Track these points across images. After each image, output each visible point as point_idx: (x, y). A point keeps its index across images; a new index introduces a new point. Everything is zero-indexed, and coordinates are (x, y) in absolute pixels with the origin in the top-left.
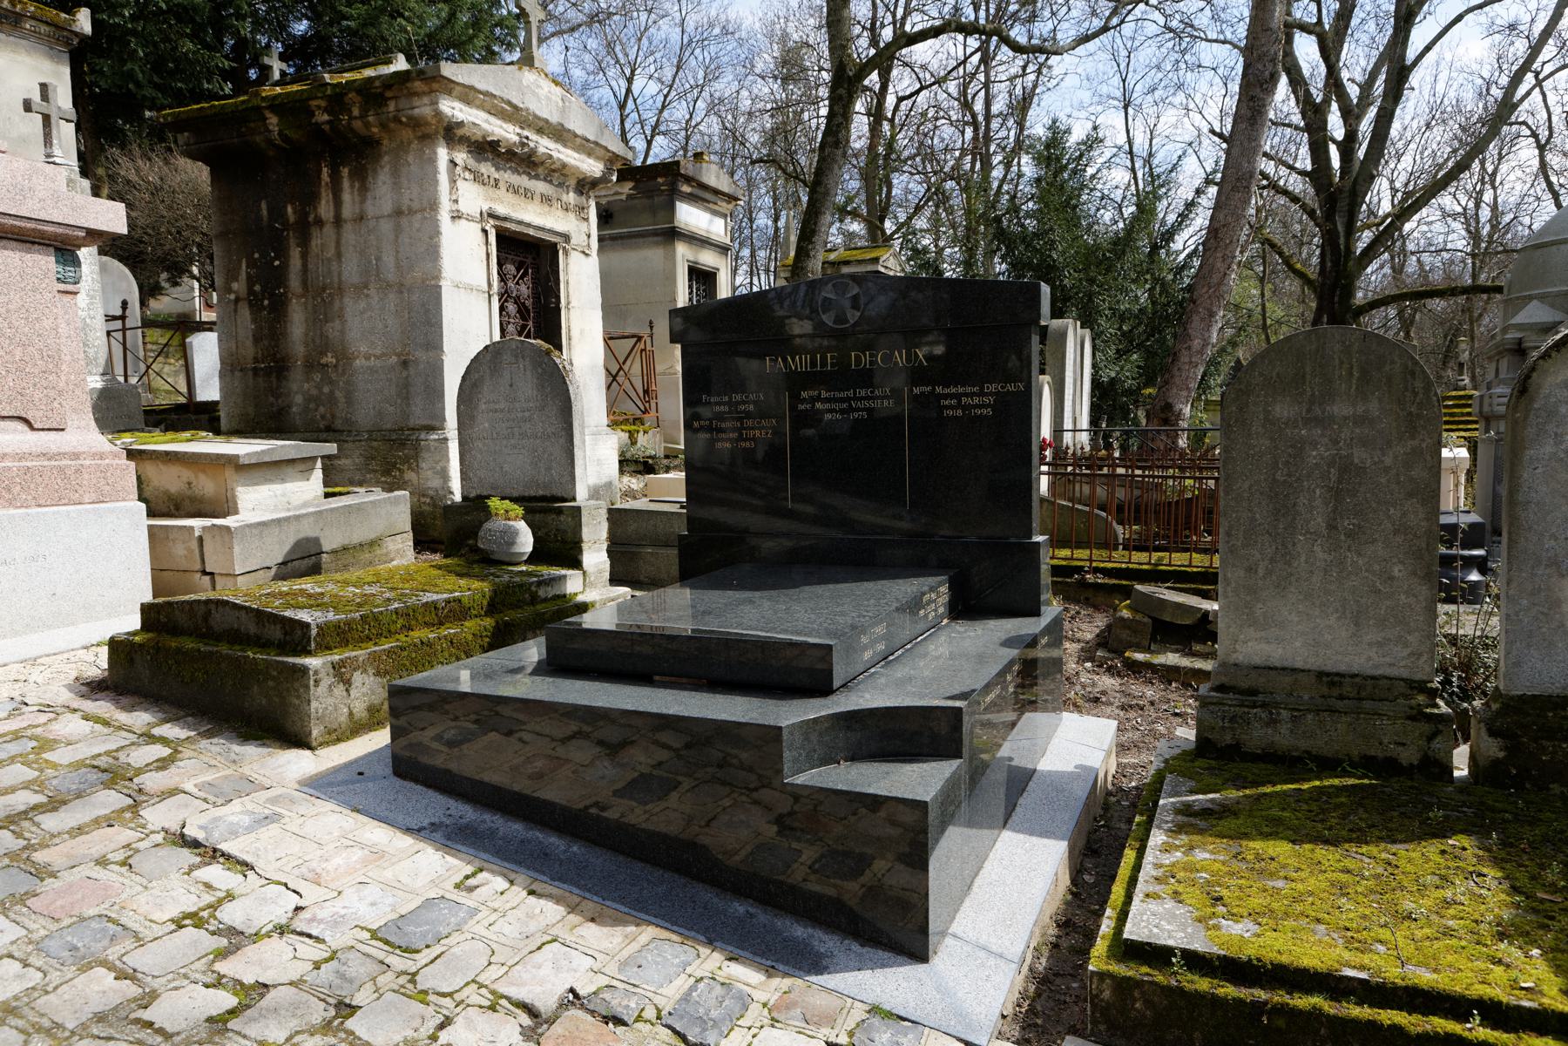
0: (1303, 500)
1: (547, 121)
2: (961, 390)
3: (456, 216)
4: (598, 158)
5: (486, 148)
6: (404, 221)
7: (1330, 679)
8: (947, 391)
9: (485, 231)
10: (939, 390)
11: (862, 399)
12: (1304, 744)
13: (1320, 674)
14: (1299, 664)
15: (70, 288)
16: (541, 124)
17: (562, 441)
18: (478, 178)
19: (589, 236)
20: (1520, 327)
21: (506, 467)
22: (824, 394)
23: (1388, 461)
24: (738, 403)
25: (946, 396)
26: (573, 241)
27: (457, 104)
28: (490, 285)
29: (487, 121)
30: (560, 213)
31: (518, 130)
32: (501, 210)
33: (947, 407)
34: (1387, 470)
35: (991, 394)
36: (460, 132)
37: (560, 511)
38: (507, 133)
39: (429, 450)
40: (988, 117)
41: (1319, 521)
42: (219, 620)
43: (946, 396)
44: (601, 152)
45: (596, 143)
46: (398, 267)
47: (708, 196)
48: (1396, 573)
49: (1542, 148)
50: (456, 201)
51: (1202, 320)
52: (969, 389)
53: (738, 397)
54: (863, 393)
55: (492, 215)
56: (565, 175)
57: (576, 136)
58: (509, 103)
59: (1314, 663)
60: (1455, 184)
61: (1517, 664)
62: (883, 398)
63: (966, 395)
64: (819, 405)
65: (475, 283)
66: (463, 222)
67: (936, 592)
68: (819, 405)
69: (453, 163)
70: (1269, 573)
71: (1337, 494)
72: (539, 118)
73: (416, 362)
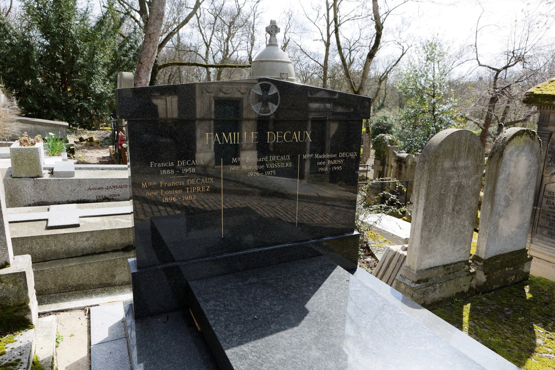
13: (444, 266)
14: (438, 265)
15: (391, 281)
33: (320, 166)
51: (145, 71)
60: (199, 9)
61: (488, 249)
67: (339, 271)
70: (435, 231)
71: (456, 197)
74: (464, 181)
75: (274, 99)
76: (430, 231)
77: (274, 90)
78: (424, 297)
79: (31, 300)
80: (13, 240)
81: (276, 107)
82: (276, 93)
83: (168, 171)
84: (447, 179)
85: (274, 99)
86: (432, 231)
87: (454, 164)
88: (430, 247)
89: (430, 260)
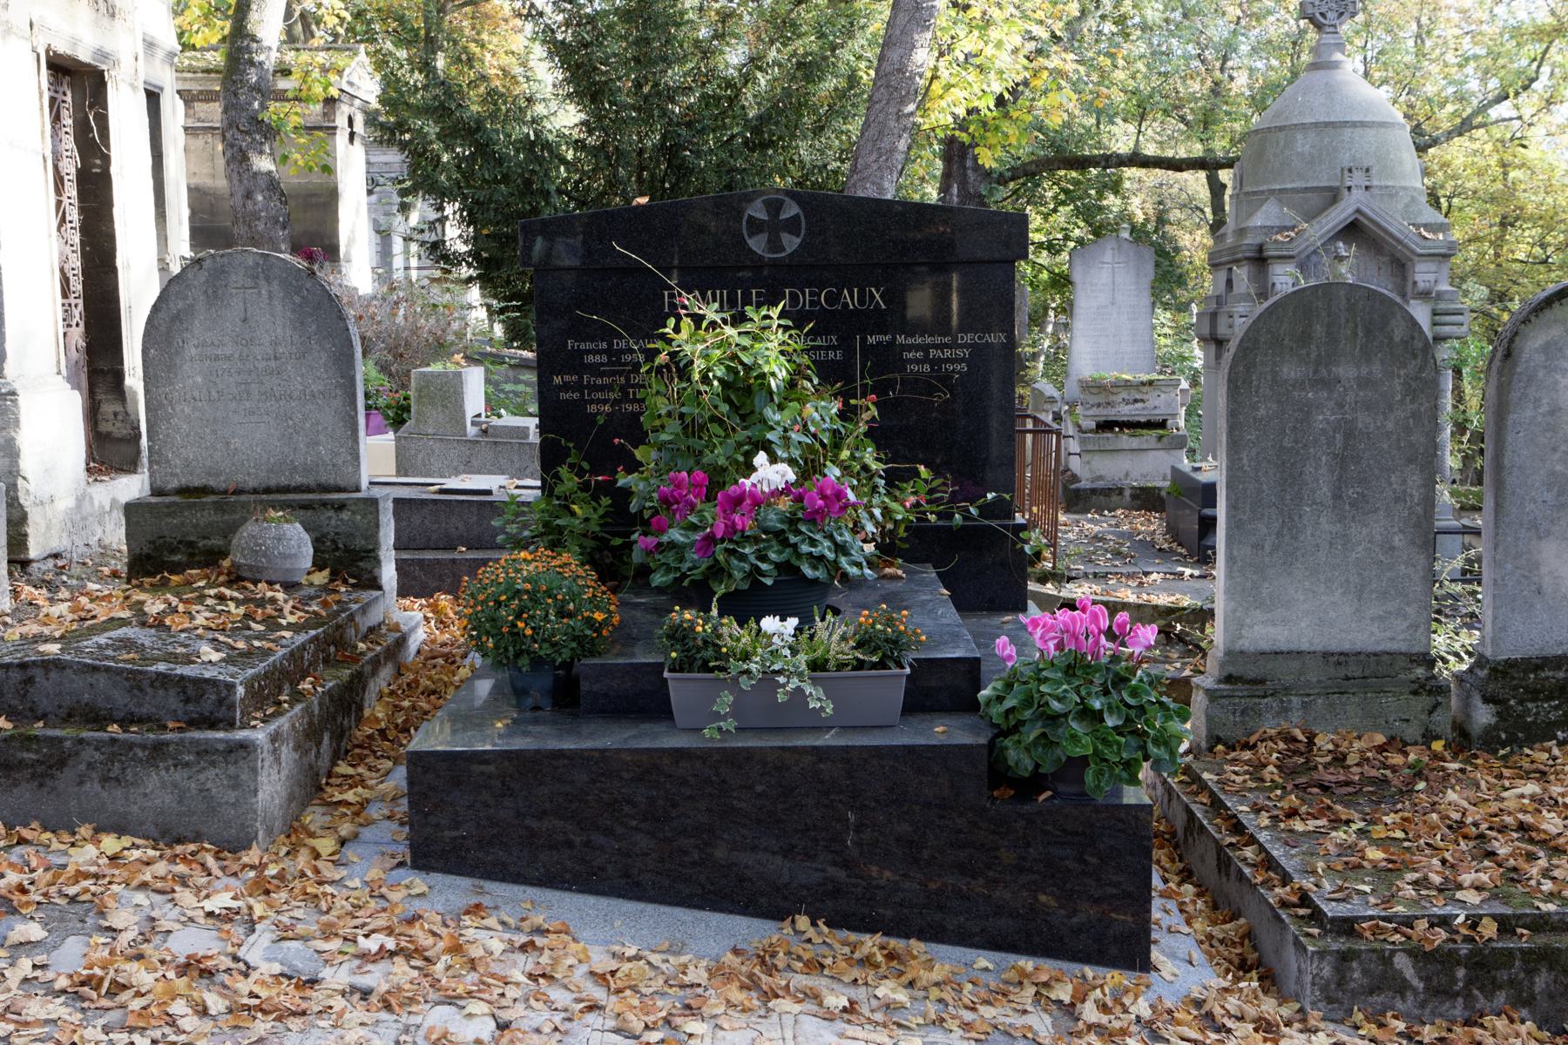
0: (1309, 469)
2: (929, 340)
8: (910, 341)
10: (901, 339)
13: (1326, 655)
14: (1305, 646)
17: (337, 403)
21: (236, 443)
23: (1390, 426)
25: (910, 348)
34: (1388, 434)
35: (965, 346)
37: (341, 507)
41: (1324, 491)
42: (45, 689)
43: (910, 348)
52: (938, 340)
59: (1319, 644)
61: (1503, 629)
62: (828, 348)
63: (936, 347)
70: (1275, 548)
71: (1341, 461)
74: (1363, 420)
75: (792, 226)
76: (1257, 546)
77: (791, 210)
78: (1243, 723)
79: (384, 547)
80: (398, 474)
81: (798, 241)
82: (797, 215)
83: (598, 357)
84: (1301, 410)
85: (792, 226)
86: (1268, 548)
87: (1315, 372)
88: (1265, 592)
89: (1271, 630)
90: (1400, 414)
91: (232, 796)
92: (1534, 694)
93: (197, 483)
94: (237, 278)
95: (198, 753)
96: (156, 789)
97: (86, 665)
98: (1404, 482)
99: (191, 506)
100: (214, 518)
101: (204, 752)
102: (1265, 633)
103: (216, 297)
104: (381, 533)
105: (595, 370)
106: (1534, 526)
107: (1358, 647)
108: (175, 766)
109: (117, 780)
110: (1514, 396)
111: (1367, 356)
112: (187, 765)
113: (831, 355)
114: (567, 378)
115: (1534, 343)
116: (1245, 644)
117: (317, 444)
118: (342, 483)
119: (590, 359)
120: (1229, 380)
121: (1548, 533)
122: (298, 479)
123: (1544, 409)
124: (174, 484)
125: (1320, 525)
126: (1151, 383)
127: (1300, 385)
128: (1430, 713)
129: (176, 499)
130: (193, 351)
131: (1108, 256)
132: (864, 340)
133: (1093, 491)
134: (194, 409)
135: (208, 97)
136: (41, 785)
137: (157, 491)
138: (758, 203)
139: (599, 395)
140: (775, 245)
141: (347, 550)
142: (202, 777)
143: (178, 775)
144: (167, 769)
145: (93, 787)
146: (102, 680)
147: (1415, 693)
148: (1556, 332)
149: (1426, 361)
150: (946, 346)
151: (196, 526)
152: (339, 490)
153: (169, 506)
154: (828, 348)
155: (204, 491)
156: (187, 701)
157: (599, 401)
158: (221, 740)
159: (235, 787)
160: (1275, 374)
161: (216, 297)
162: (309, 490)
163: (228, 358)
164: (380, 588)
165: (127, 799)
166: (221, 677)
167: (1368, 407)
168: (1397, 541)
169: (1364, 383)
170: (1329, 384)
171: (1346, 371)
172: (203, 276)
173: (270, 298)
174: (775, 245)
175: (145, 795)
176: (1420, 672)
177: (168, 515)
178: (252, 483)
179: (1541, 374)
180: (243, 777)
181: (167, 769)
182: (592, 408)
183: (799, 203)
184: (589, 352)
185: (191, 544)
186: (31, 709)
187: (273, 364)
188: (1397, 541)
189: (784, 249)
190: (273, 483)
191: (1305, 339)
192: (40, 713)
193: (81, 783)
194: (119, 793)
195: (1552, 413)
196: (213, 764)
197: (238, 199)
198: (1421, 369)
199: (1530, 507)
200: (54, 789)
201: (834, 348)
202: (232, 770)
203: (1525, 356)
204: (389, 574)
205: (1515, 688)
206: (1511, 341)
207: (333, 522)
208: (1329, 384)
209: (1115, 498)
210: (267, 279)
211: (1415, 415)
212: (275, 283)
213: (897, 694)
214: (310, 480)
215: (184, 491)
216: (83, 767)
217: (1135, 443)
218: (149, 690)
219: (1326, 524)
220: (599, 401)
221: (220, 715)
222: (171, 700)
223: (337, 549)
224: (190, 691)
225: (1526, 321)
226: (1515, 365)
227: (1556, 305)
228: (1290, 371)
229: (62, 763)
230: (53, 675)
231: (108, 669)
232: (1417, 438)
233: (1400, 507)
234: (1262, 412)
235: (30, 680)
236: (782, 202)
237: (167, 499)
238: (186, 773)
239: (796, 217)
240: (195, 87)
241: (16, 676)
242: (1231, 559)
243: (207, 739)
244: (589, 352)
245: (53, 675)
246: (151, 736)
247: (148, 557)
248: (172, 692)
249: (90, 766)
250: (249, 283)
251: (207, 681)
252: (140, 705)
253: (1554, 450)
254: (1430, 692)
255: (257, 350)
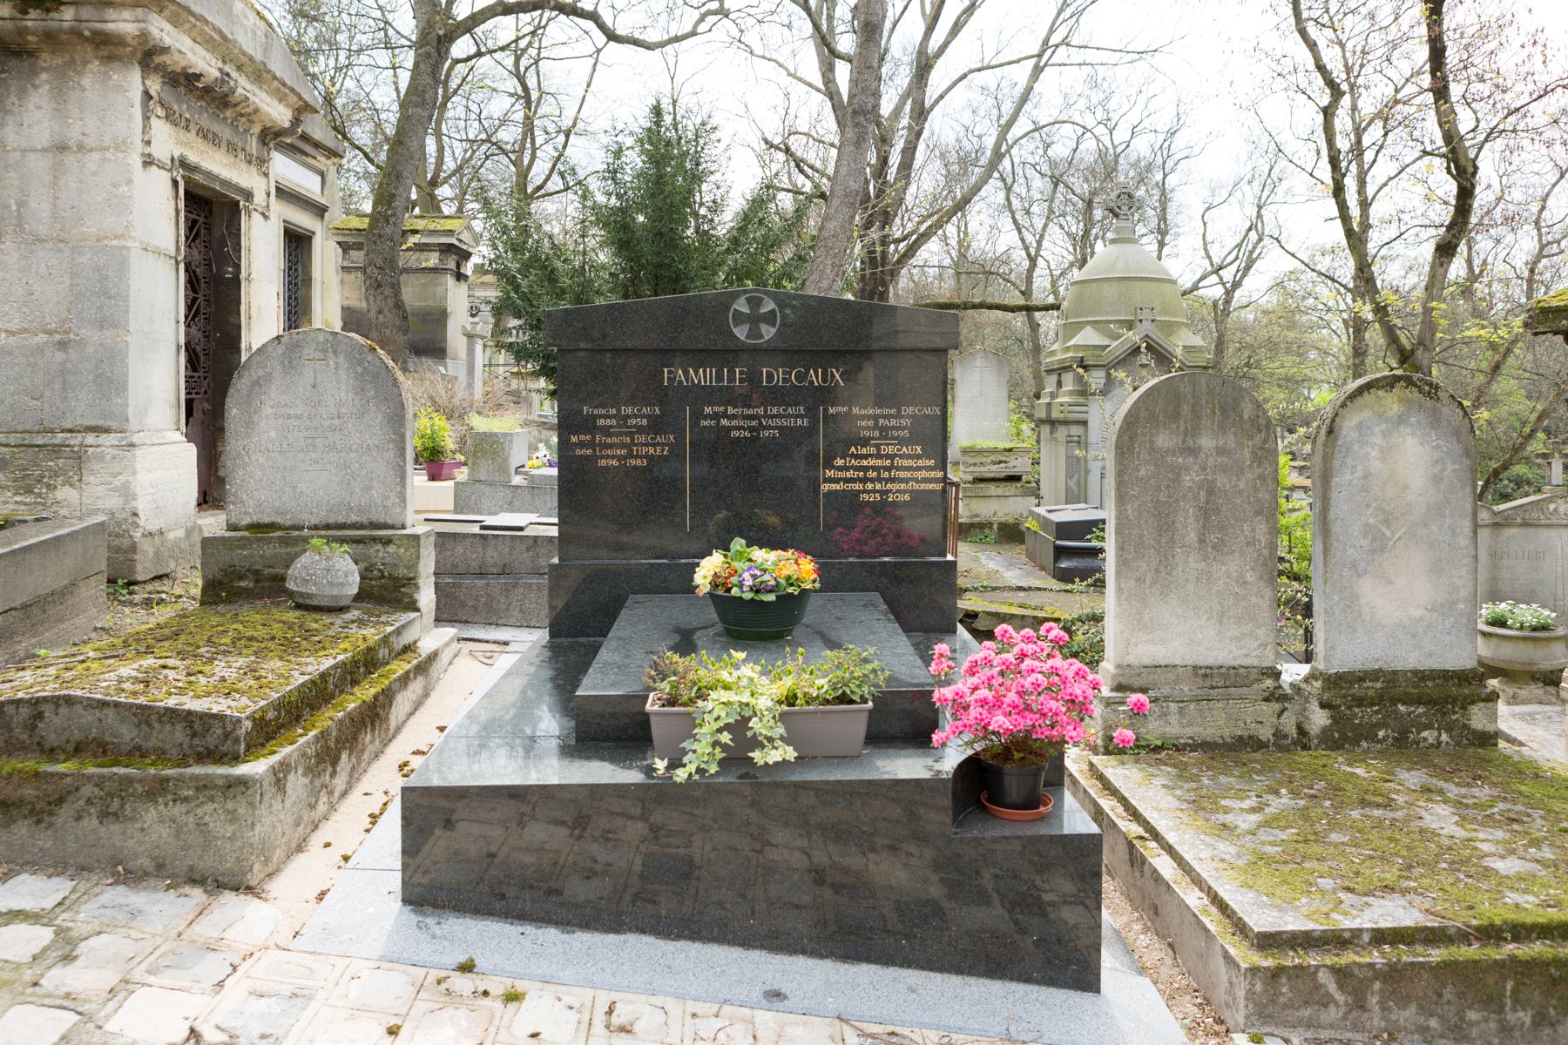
0: (1180, 518)
1: (251, 58)
2: (878, 412)
3: (149, 162)
4: (287, 106)
5: (184, 81)
6: (70, 159)
7: (1205, 674)
8: (864, 412)
9: (175, 183)
10: (855, 410)
11: (774, 416)
12: (1189, 731)
14: (1177, 662)
16: (244, 59)
17: (390, 455)
18: (169, 117)
19: (268, 195)
20: (1077, 347)
21: (302, 487)
22: (730, 410)
23: (1242, 485)
24: (628, 417)
25: (863, 418)
26: (256, 200)
27: (168, 27)
28: (178, 248)
29: (192, 50)
30: (243, 165)
31: (220, 65)
32: (193, 158)
34: (1240, 492)
35: (908, 416)
36: (158, 59)
37: (387, 542)
38: (205, 63)
39: (101, 457)
40: (455, 92)
41: (1192, 537)
42: (54, 727)
43: (863, 418)
44: (293, 99)
45: (292, 90)
46: (55, 215)
47: (308, 149)
48: (1249, 579)
49: (1008, 189)
50: (148, 143)
52: (886, 411)
53: (629, 411)
54: (775, 411)
55: (184, 164)
56: (251, 122)
57: (275, 78)
58: (220, 32)
59: (1191, 660)
61: (1333, 648)
62: (797, 416)
63: (884, 417)
64: (724, 422)
65: (163, 246)
66: (154, 168)
68: (724, 422)
69: (147, 96)
70: (1154, 582)
71: (1205, 512)
72: (244, 54)
73: (81, 344)
74: (1222, 480)
75: (770, 318)
80: (455, 511)
81: (773, 330)
85: (770, 318)
88: (1146, 617)
90: (1250, 476)
91: (229, 830)
92: (1360, 701)
93: (266, 520)
94: (309, 352)
95: (197, 789)
96: (154, 826)
97: (99, 701)
98: (1253, 530)
99: (259, 540)
100: (279, 550)
101: (203, 786)
102: (1147, 651)
103: (291, 367)
104: (421, 564)
105: (606, 431)
106: (1354, 566)
107: (1220, 662)
108: (174, 801)
109: (115, 814)
110: (1336, 463)
111: (1223, 429)
112: (186, 800)
113: (799, 422)
114: (582, 437)
115: (1349, 425)
116: (1131, 659)
117: (370, 488)
118: (390, 522)
119: (601, 422)
120: (1117, 447)
121: (1365, 571)
122: (354, 518)
123: (1359, 474)
124: (247, 521)
125: (1189, 564)
126: (1010, 450)
127: (1171, 452)
128: (1279, 716)
129: (246, 534)
130: (269, 411)
131: (978, 362)
132: (826, 410)
133: (972, 525)
134: (268, 459)
135: (359, 246)
136: (39, 822)
137: (233, 527)
138: (742, 300)
139: (609, 452)
140: (755, 333)
141: (391, 577)
142: (199, 812)
143: (178, 810)
144: (166, 805)
145: (90, 823)
146: (110, 713)
147: (1266, 700)
148: (1366, 414)
149: (1268, 435)
150: (892, 416)
151: (262, 557)
152: (392, 527)
153: (240, 539)
154: (797, 416)
155: (273, 526)
156: (194, 735)
157: (608, 457)
158: (221, 776)
159: (234, 820)
160: (1152, 442)
161: (291, 367)
162: (361, 527)
163: (299, 417)
164: (418, 610)
165: (124, 833)
166: (228, 712)
167: (1224, 470)
168: (1250, 577)
169: (1221, 451)
170: (1193, 452)
171: (1206, 442)
172: (281, 349)
173: (337, 368)
174: (755, 333)
175: (143, 830)
176: (1269, 683)
177: (240, 547)
178: (314, 521)
179: (1355, 447)
180: (241, 811)
181: (166, 805)
182: (603, 463)
183: (775, 301)
184: (601, 416)
185: (257, 573)
186: (39, 743)
187: (336, 422)
188: (1250, 577)
189: (762, 337)
190: (331, 521)
191: (1175, 415)
192: (47, 747)
193: (79, 818)
194: (115, 828)
195: (1365, 477)
196: (212, 799)
197: (373, 314)
198: (1265, 441)
199: (1351, 551)
200: (51, 825)
201: (802, 416)
202: (230, 805)
203: (1344, 432)
204: (426, 597)
205: (1345, 696)
206: (1333, 420)
207: (381, 554)
208: (1193, 452)
209: (987, 531)
210: (335, 352)
211: (1262, 477)
212: (342, 356)
213: (859, 727)
214: (364, 519)
215: (255, 527)
216: (82, 802)
217: (999, 491)
218: (156, 725)
219: (1194, 563)
220: (608, 457)
221: (224, 749)
222: (178, 734)
223: (383, 577)
224: (197, 727)
225: (1343, 405)
226: (1336, 439)
227: (1366, 394)
228: (1164, 440)
229: (61, 800)
230: (63, 710)
231: (117, 705)
232: (1263, 495)
233: (1251, 549)
234: (1142, 473)
235: (39, 716)
236: (761, 300)
237: (239, 534)
238: (183, 808)
239: (773, 312)
240: (351, 240)
241: (25, 711)
242: (1119, 590)
243: (207, 775)
244: (601, 416)
245: (63, 710)
246: (152, 771)
247: (220, 583)
248: (179, 727)
249: (89, 801)
250: (318, 355)
251: (214, 716)
252: (147, 739)
253: (1368, 506)
254: (1278, 700)
255: (323, 410)
